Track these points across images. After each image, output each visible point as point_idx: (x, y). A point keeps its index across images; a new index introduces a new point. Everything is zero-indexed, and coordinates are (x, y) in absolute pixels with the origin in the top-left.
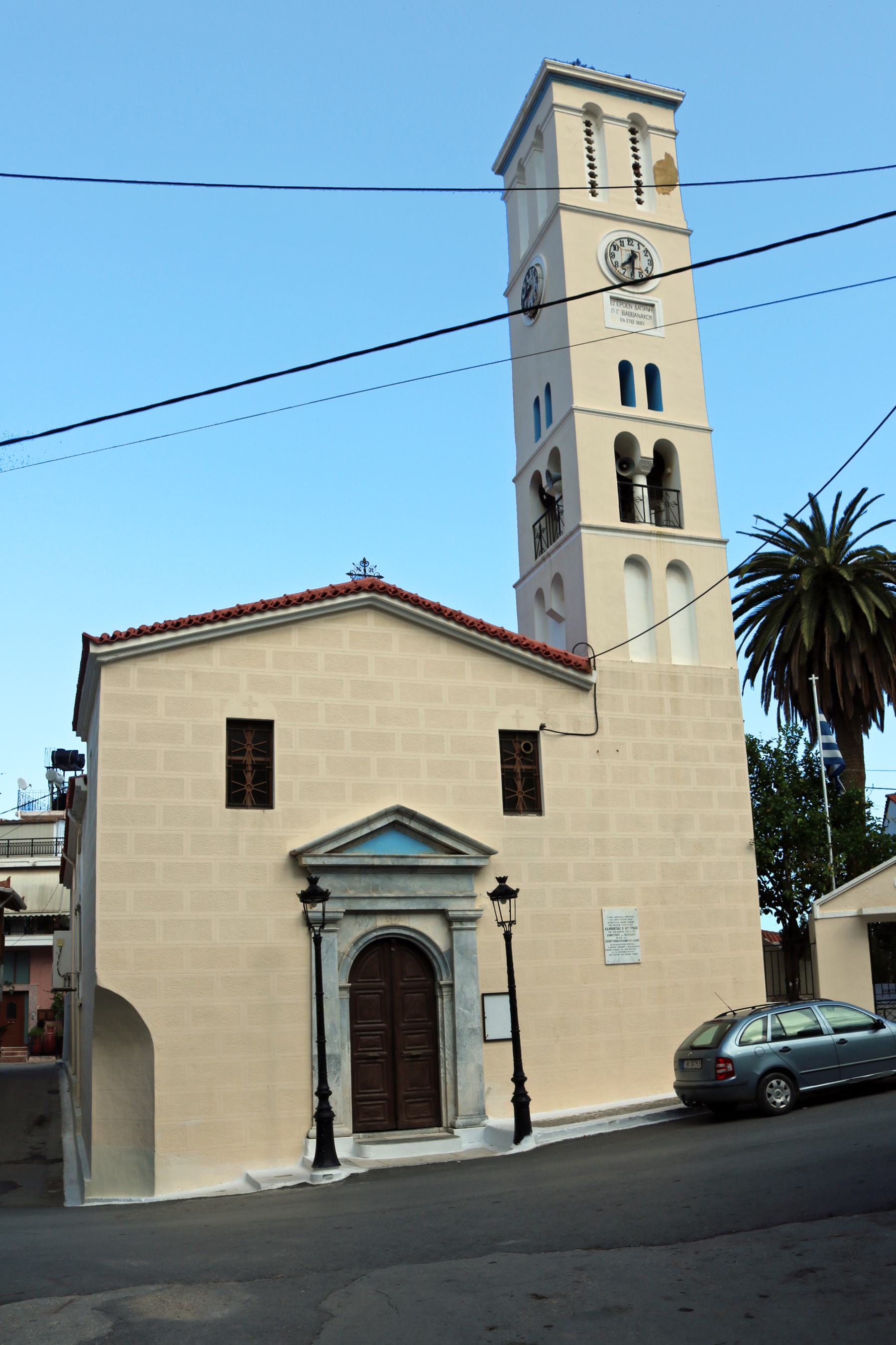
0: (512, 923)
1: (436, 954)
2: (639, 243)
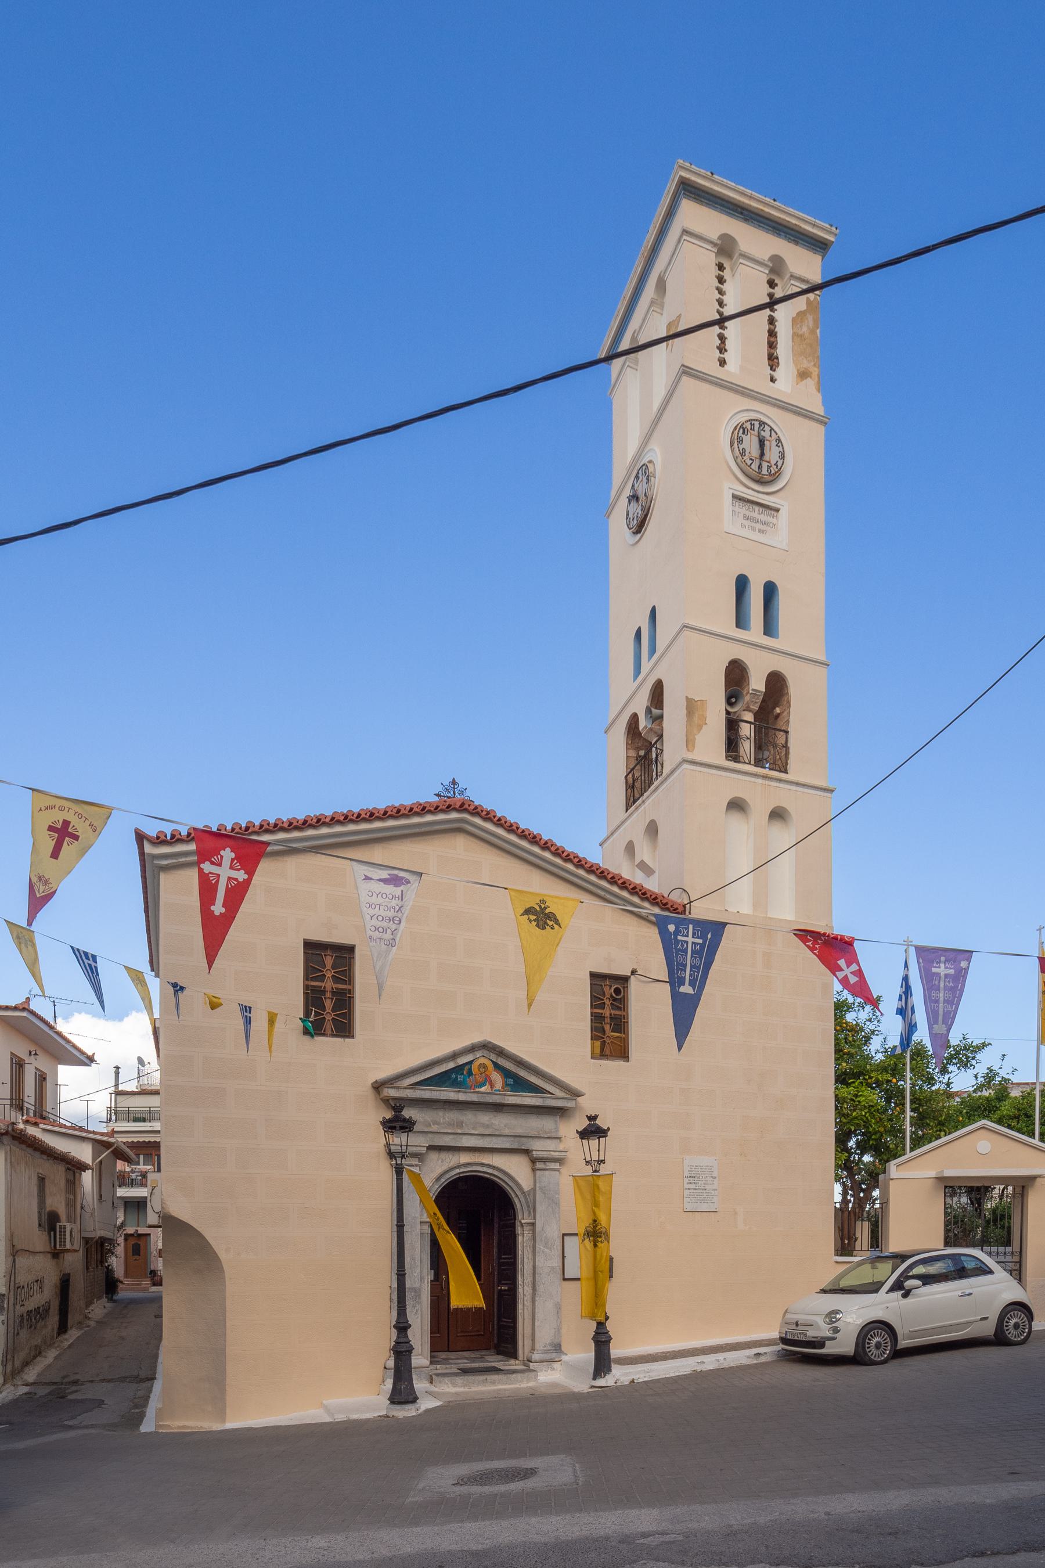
0: (601, 1162)
1: (519, 1193)
2: (772, 429)
